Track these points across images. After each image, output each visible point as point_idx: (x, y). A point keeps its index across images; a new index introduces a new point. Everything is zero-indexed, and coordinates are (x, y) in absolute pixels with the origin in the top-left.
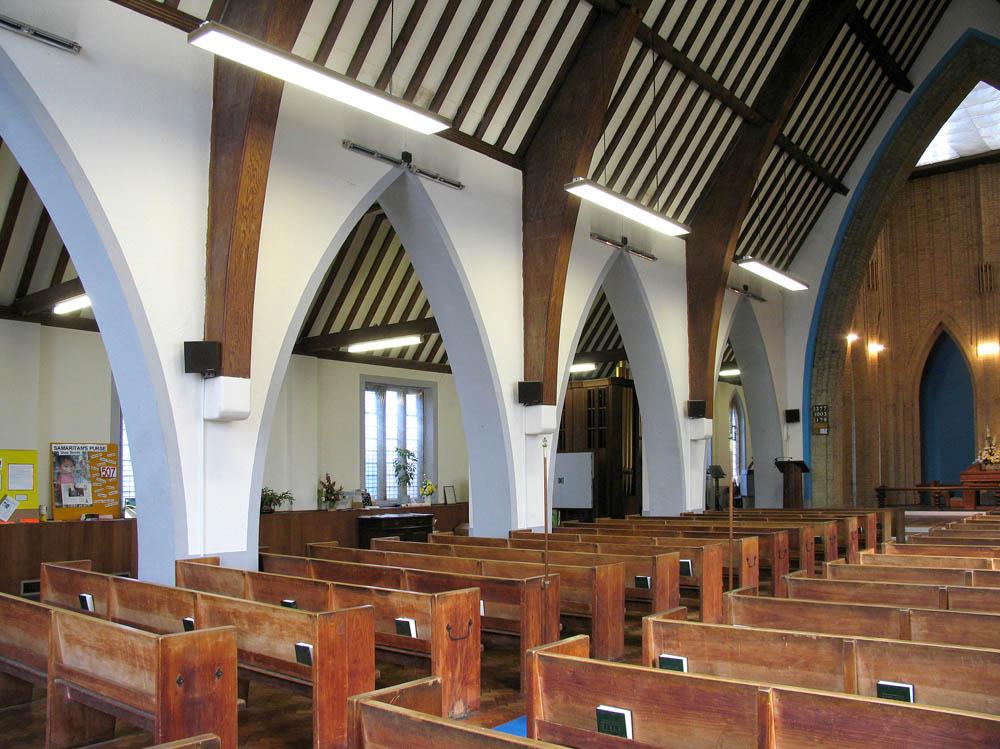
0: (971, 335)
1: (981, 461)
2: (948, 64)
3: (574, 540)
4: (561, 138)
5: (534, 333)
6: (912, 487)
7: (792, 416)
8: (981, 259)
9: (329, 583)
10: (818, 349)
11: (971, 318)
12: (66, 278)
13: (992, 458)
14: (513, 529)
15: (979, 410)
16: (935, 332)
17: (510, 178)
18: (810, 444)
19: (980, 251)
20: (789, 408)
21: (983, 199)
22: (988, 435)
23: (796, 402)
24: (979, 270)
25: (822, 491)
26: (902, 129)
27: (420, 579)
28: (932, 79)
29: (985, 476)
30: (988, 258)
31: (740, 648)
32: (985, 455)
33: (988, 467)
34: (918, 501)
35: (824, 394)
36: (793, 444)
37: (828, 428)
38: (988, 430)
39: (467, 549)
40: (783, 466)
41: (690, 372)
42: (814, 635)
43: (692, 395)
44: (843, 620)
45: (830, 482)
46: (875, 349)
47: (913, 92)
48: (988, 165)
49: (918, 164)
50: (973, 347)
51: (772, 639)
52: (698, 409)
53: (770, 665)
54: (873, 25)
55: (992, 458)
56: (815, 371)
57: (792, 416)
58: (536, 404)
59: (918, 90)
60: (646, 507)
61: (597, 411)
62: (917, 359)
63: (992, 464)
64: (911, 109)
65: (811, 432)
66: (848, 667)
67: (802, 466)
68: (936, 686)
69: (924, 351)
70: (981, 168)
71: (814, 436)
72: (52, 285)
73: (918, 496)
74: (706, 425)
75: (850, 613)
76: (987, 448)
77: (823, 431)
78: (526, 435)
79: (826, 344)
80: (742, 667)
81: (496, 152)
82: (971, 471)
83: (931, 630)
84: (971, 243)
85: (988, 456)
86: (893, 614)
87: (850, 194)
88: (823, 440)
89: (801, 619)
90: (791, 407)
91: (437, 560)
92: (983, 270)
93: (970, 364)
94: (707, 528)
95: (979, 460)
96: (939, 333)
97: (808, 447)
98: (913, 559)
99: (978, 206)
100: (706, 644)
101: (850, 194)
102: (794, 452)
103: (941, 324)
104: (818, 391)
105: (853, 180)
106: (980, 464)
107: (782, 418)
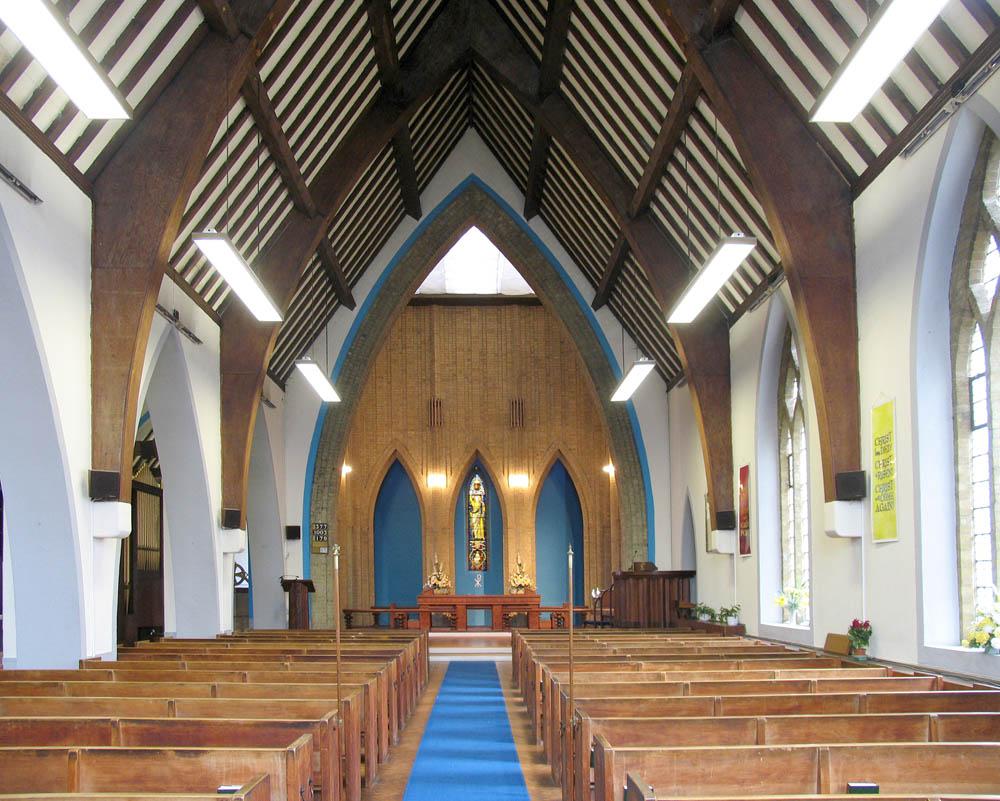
2: (452, 202)
4: (151, 173)
5: (106, 411)
6: (368, 609)
7: (293, 533)
9: (76, 749)
14: (83, 658)
16: (389, 460)
17: (76, 205)
19: (432, 385)
20: (289, 525)
23: (294, 516)
25: (324, 612)
26: (408, 255)
27: (147, 730)
31: (712, 769)
32: (434, 580)
33: (436, 591)
34: (373, 623)
35: (324, 512)
36: (293, 562)
39: (90, 686)
40: (287, 585)
41: (222, 477)
42: (789, 747)
43: (225, 503)
44: (703, 734)
45: (329, 603)
46: (346, 470)
47: (421, 220)
48: (523, 307)
49: (418, 292)
50: (505, 478)
51: (747, 756)
52: (231, 520)
53: (742, 782)
55: (440, 583)
57: (293, 533)
58: (109, 500)
59: (426, 219)
60: (171, 627)
62: (373, 485)
63: (439, 588)
65: (310, 552)
66: (825, 774)
67: (309, 585)
68: (894, 781)
69: (381, 472)
70: (435, 308)
73: (372, 617)
74: (239, 537)
75: (711, 726)
78: (94, 538)
80: (712, 788)
81: (66, 162)
83: (781, 735)
85: (436, 580)
86: (750, 724)
87: (357, 309)
88: (323, 558)
89: (662, 737)
90: (291, 523)
91: (96, 702)
92: (434, 405)
94: (300, 652)
96: (393, 460)
97: (308, 565)
98: (597, 675)
99: (432, 344)
100: (675, 768)
101: (357, 309)
102: (295, 571)
104: (318, 508)
105: (362, 292)
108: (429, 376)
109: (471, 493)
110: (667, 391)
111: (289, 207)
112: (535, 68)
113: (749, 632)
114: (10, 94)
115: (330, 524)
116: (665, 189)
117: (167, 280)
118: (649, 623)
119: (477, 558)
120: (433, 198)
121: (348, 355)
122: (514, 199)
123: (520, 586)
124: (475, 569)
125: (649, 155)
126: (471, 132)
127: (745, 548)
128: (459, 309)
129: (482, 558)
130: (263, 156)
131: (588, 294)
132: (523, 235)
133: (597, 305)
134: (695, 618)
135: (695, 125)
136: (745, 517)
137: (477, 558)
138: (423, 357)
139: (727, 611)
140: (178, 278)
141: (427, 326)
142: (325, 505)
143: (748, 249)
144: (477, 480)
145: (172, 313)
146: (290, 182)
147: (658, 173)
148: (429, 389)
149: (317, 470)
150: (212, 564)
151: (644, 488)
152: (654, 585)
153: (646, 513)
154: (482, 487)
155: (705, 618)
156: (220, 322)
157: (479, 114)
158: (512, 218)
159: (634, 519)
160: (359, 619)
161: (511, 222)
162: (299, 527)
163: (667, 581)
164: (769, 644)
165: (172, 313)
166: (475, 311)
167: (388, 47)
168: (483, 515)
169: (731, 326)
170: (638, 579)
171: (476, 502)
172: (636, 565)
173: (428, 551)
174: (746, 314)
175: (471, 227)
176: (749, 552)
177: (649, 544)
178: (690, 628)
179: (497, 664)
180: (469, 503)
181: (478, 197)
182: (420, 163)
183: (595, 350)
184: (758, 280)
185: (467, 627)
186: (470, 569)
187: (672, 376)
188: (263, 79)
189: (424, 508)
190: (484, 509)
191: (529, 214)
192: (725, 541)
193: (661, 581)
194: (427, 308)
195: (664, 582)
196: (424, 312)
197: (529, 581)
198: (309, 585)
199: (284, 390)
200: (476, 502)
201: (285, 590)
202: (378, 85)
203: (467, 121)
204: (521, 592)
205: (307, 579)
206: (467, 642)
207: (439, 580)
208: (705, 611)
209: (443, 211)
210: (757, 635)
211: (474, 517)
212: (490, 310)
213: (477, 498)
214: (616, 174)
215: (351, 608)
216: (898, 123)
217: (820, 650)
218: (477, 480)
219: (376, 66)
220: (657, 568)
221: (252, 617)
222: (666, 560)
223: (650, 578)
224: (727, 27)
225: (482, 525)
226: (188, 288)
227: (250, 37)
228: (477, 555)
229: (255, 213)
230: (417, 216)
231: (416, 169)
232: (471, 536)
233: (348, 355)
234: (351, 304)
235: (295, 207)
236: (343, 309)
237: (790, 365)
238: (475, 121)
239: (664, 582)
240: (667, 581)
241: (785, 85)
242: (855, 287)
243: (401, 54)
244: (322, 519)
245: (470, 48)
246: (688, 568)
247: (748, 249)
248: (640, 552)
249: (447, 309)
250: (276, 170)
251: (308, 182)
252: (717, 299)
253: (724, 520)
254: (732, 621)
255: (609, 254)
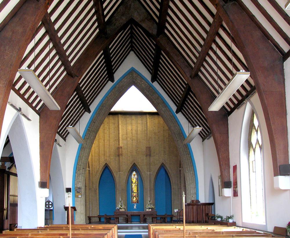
3: (32, 234)
4: (5, 50)
7: (68, 190)
8: (119, 145)
10: (78, 167)
15: (117, 192)
21: (120, 126)
23: (69, 184)
26: (110, 95)
28: (120, 80)
30: (121, 145)
32: (120, 206)
33: (121, 210)
34: (98, 221)
36: (69, 200)
37: (81, 195)
38: (120, 199)
43: (41, 179)
47: (114, 83)
48: (150, 115)
52: (43, 185)
54: (67, 54)
55: (122, 207)
56: (77, 174)
57: (68, 190)
61: (148, 174)
64: (113, 88)
65: (75, 196)
70: (120, 116)
71: (76, 198)
72: (210, 27)
76: (120, 204)
77: (80, 196)
79: (81, 165)
81: (34, 109)
87: (91, 113)
88: (79, 199)
97: (74, 201)
101: (91, 113)
105: (93, 107)
107: (65, 190)
108: (117, 138)
109: (132, 177)
110: (203, 141)
111: (65, 73)
112: (155, 25)
113: (237, 224)
114: (29, 101)
115: (82, 187)
116: (191, 95)
117: (12, 92)
118: (197, 221)
119: (135, 199)
120: (118, 75)
121: (88, 129)
122: (147, 76)
123: (150, 208)
124: (134, 203)
125: (183, 92)
126: (132, 53)
127: (235, 194)
128: (128, 116)
129: (136, 199)
130: (80, 102)
131: (174, 108)
132: (151, 88)
133: (177, 112)
134: (215, 219)
135: (218, 40)
136: (236, 184)
137: (135, 199)
138: (115, 132)
139: (229, 217)
140: (17, 92)
141: (117, 121)
142: (80, 181)
143: (201, 128)
144: (134, 173)
145: (18, 109)
146: (65, 63)
147: (202, 60)
148: (117, 143)
149: (77, 168)
150: (35, 201)
151: (195, 175)
152: (199, 208)
153: (196, 183)
154: (136, 175)
155: (219, 219)
156: (39, 114)
157: (136, 34)
158: (147, 82)
159: (191, 185)
160: (93, 220)
161: (146, 84)
162: (71, 188)
163: (204, 206)
164: (249, 230)
165: (18, 109)
166: (134, 117)
167: (101, 15)
168: (136, 185)
169: (229, 116)
170: (193, 206)
171: (134, 180)
172: (193, 201)
173: (118, 196)
174: (236, 110)
175: (132, 86)
176: (237, 196)
177: (197, 194)
178: (214, 223)
179: (142, 235)
180: (132, 180)
181: (135, 75)
182: (115, 70)
183: (177, 127)
184: (236, 102)
185: (131, 222)
186: (132, 203)
187: (206, 134)
188: (53, 21)
189: (116, 182)
190: (137, 183)
191: (153, 81)
192: (228, 192)
193: (202, 206)
194: (117, 116)
195: (203, 207)
196: (116, 117)
197: (153, 206)
198: (74, 208)
199: (65, 141)
200: (134, 180)
201: (66, 210)
202: (98, 30)
203: (130, 49)
204: (150, 210)
205: (74, 206)
206: (132, 228)
207: (121, 206)
208: (219, 217)
209: (122, 80)
210: (241, 226)
211: (134, 185)
212: (139, 116)
213: (134, 179)
214: (186, 62)
215: (91, 216)
216: (244, 93)
217: (272, 233)
218: (134, 173)
219: (104, 60)
220: (200, 202)
221: (54, 220)
222: (202, 200)
223: (197, 205)
224: (197, 75)
225: (136, 188)
226: (22, 96)
227: (78, 77)
228: (135, 198)
229: (48, 70)
230: (113, 81)
231: (112, 60)
232: (132, 191)
233: (88, 129)
234: (89, 111)
235: (42, 22)
236: (86, 113)
237: (253, 128)
238: (133, 49)
239: (203, 207)
240: (204, 206)
241: (256, 19)
242: (285, 95)
243: (106, 19)
244: (79, 185)
245: (132, 18)
246: (211, 202)
247: (201, 128)
248: (194, 196)
249: (124, 116)
250: (59, 58)
251: (72, 64)
252: (223, 107)
253: (227, 184)
254: (231, 221)
255: (179, 102)
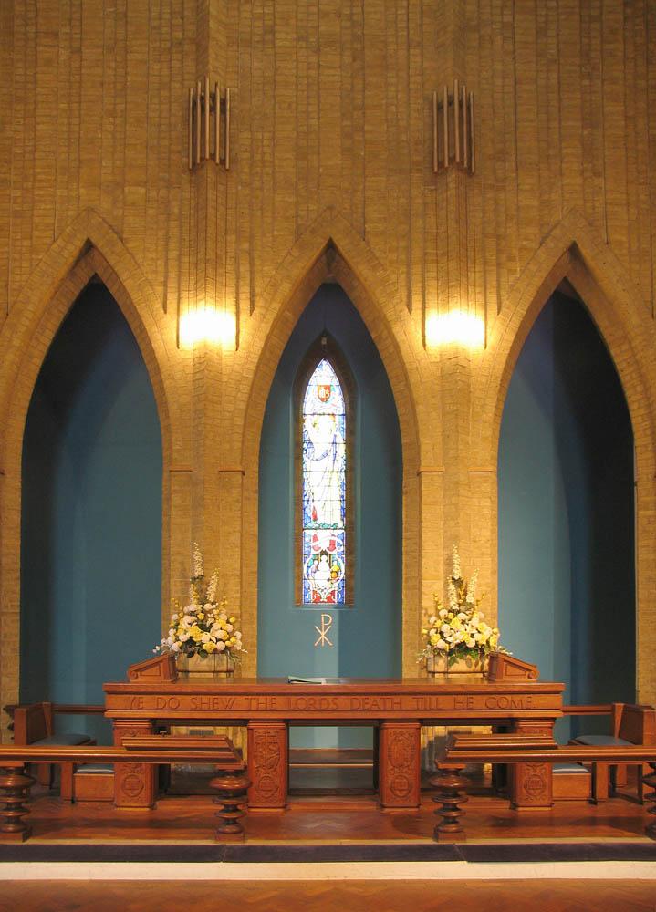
0: (165, 284)
1: (176, 647)
11: (167, 239)
12: (637, 798)
13: (205, 637)
15: (176, 499)
18: (257, 711)
19: (201, 60)
22: (198, 572)
24: (195, 106)
29: (186, 701)
32: (187, 629)
33: (195, 662)
38: (197, 556)
50: (169, 321)
55: (205, 637)
63: (204, 653)
82: (143, 681)
84: (179, 35)
85: (194, 632)
93: (157, 369)
95: (171, 642)
103: (89, 246)
105: (30, 842)
106: (172, 658)
